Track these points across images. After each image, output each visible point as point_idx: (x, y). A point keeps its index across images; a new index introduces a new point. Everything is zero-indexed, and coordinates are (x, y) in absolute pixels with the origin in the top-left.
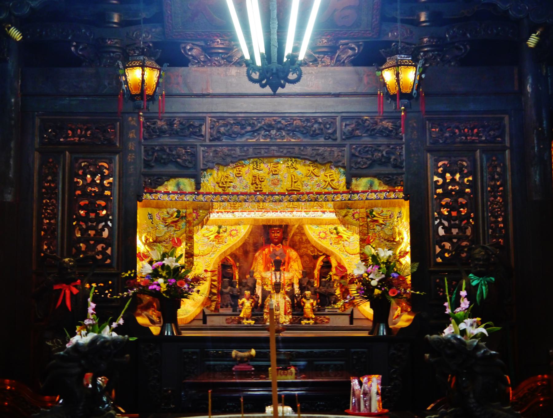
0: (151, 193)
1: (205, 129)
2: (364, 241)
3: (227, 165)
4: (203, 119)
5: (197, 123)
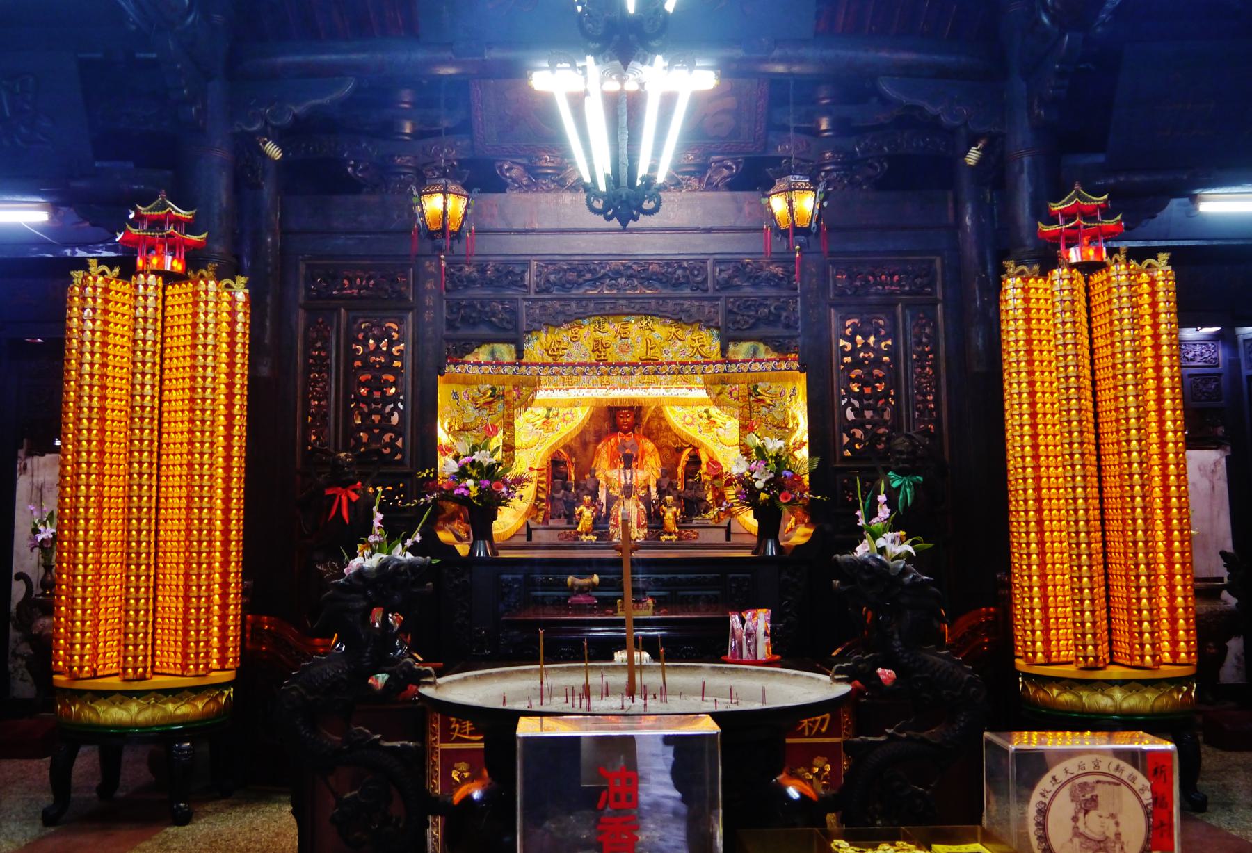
0: (456, 364)
1: (530, 278)
2: (746, 428)
3: (559, 326)
4: (527, 263)
5: (518, 269)
